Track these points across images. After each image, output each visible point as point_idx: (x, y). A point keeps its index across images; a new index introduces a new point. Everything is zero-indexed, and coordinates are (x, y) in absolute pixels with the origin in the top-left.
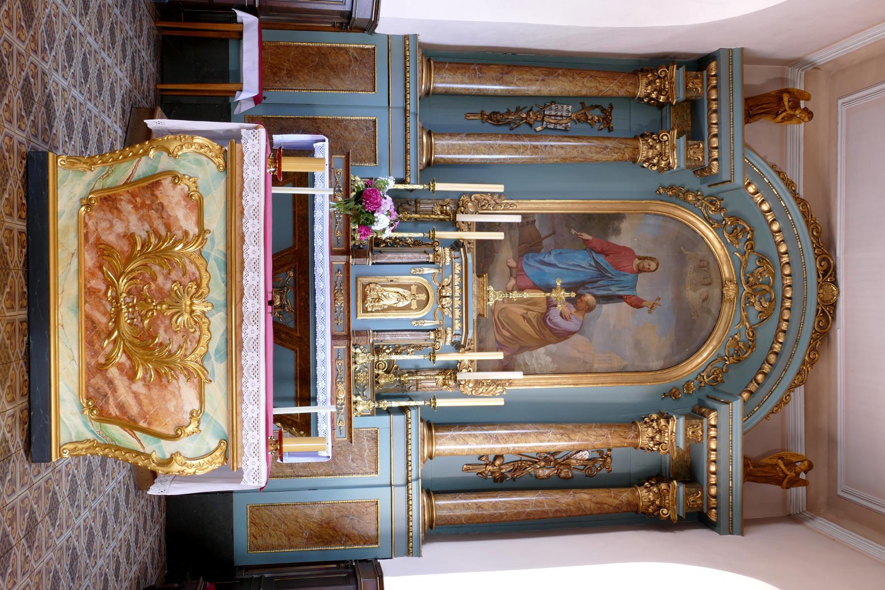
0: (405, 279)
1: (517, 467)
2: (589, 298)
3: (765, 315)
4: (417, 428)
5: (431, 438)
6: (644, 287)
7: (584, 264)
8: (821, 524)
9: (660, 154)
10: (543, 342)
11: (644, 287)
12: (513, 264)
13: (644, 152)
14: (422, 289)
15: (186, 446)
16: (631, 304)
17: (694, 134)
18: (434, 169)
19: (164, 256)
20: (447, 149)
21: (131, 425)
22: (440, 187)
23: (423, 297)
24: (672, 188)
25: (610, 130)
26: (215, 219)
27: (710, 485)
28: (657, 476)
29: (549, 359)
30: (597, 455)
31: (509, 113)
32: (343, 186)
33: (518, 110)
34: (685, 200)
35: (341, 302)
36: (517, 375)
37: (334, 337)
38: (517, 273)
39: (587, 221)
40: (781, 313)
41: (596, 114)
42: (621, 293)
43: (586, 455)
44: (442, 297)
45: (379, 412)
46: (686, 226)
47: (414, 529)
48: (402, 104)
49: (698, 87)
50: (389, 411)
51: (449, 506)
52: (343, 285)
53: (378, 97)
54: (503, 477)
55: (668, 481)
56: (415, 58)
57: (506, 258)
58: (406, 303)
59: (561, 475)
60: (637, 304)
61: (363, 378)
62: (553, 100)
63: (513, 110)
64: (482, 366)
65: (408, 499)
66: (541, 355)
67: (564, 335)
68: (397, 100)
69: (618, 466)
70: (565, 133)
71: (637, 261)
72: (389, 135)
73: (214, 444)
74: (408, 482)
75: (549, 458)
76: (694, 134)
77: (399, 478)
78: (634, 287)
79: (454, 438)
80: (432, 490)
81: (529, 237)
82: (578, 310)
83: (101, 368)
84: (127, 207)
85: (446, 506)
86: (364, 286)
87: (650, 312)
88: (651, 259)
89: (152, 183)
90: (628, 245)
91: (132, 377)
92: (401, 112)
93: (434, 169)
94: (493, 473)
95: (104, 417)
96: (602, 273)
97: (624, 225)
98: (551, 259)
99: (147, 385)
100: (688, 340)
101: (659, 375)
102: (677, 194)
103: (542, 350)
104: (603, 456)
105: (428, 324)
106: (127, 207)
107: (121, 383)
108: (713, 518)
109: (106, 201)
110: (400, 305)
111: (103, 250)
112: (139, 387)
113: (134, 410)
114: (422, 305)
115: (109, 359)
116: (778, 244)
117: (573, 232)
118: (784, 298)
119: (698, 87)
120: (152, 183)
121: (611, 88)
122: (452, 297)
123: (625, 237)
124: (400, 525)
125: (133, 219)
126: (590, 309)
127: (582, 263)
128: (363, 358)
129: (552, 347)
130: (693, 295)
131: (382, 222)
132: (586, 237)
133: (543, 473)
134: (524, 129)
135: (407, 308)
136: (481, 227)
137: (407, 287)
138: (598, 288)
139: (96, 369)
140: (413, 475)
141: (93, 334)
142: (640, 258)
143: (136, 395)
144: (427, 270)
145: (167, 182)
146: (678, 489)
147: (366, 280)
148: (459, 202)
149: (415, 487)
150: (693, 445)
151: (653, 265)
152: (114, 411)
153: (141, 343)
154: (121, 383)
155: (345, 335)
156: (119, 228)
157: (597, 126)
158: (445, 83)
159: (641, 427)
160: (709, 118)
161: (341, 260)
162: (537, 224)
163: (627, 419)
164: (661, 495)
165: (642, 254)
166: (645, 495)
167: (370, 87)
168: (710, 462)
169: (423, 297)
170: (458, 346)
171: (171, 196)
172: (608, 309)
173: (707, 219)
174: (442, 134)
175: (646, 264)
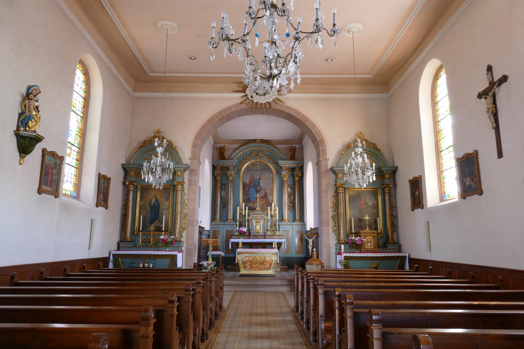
0: (255, 225)
1: (291, 203)
3: (262, 153)
4: (282, 223)
6: (257, 178)
8: (303, 143)
11: (257, 178)
13: (231, 178)
14: (256, 222)
15: (273, 259)
17: (228, 168)
18: (234, 219)
19: (251, 261)
20: (230, 216)
21: (271, 265)
22: (238, 219)
26: (248, 255)
28: (293, 176)
32: (238, 237)
35: (259, 237)
36: (273, 204)
37: (265, 238)
38: (254, 203)
41: (224, 187)
43: (289, 189)
45: (279, 230)
49: (218, 168)
50: (279, 228)
51: (297, 217)
52: (256, 237)
53: (221, 230)
55: (294, 174)
56: (214, 223)
57: (251, 205)
59: (292, 195)
60: (260, 179)
61: (273, 233)
62: (221, 195)
64: (271, 209)
66: (270, 198)
67: (266, 194)
68: (222, 226)
69: (292, 183)
70: (228, 193)
72: (229, 228)
75: (289, 197)
76: (228, 168)
77: (291, 226)
80: (294, 220)
81: (247, 200)
85: (297, 217)
89: (243, 262)
93: (234, 219)
95: (270, 268)
96: (254, 186)
97: (245, 181)
100: (268, 169)
102: (239, 171)
104: (289, 186)
109: (245, 267)
111: (251, 268)
114: (259, 222)
119: (218, 168)
120: (243, 262)
121: (219, 185)
123: (247, 181)
126: (261, 188)
127: (252, 190)
128: (269, 233)
130: (259, 168)
131: (245, 230)
133: (292, 198)
134: (226, 201)
136: (245, 209)
139: (264, 269)
141: (260, 269)
146: (296, 172)
148: (241, 214)
149: (293, 223)
153: (262, 263)
155: (265, 236)
158: (218, 217)
161: (251, 237)
163: (282, 183)
164: (296, 176)
166: (297, 179)
170: (267, 215)
171: (245, 260)
172: (261, 185)
173: (244, 165)
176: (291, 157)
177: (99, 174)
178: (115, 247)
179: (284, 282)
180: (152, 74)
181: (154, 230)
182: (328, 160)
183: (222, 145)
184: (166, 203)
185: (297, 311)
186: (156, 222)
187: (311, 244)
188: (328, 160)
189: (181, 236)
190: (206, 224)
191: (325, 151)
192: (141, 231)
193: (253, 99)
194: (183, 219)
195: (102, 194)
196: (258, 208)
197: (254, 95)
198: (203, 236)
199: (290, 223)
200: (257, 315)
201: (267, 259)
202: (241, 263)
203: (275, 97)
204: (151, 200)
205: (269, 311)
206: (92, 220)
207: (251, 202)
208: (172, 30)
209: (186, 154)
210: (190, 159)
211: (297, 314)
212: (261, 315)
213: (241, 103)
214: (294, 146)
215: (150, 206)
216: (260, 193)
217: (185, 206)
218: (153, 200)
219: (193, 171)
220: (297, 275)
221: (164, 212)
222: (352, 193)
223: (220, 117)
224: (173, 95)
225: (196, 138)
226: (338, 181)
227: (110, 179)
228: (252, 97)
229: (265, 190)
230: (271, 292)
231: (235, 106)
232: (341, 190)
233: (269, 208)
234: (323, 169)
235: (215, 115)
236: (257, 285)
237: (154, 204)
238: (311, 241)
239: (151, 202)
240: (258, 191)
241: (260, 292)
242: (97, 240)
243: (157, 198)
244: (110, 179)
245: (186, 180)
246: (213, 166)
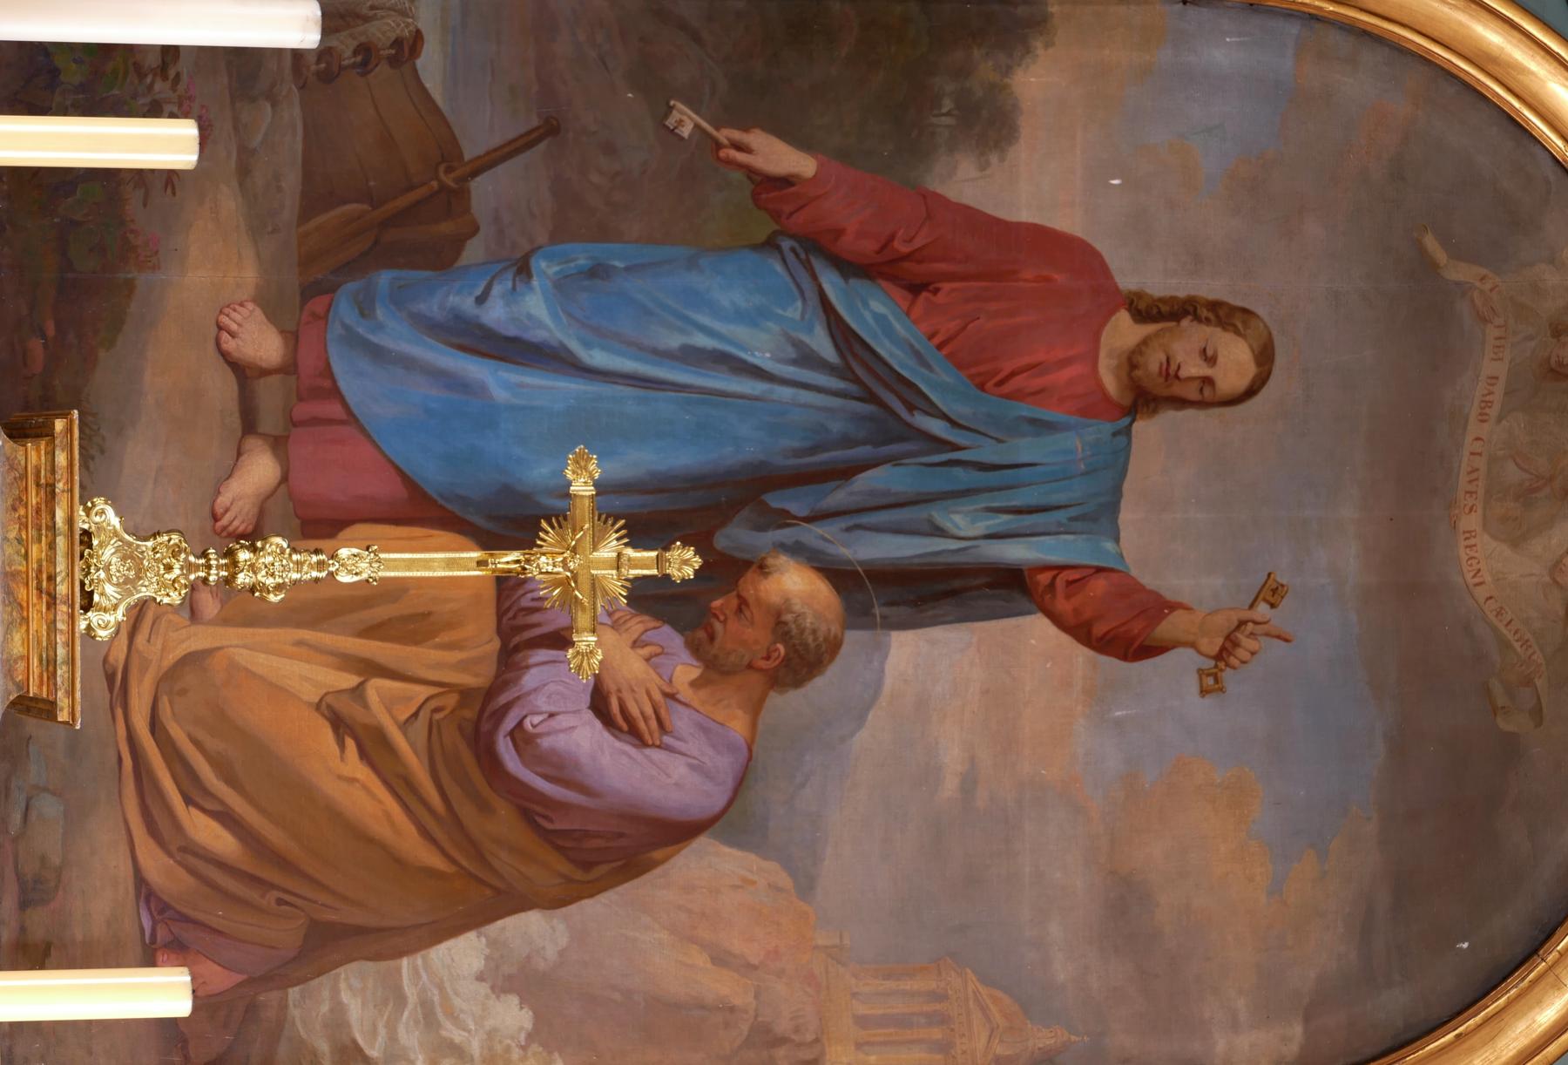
2: (794, 584)
6: (1171, 516)
11: (1171, 516)
12: (261, 342)
16: (1081, 631)
38: (288, 405)
42: (1016, 552)
57: (215, 298)
60: (1124, 628)
67: (613, 847)
71: (1123, 332)
78: (1101, 514)
82: (715, 669)
88: (1224, 315)
96: (882, 404)
98: (534, 309)
103: (463, 954)
117: (686, 120)
126: (800, 660)
129: (533, 931)
132: (776, 155)
142: (1146, 310)
151: (1234, 360)
172: (922, 660)
175: (1185, 348)
176: (48, 719)
207: (308, 289)
229: (732, 818)
236: (642, 713)
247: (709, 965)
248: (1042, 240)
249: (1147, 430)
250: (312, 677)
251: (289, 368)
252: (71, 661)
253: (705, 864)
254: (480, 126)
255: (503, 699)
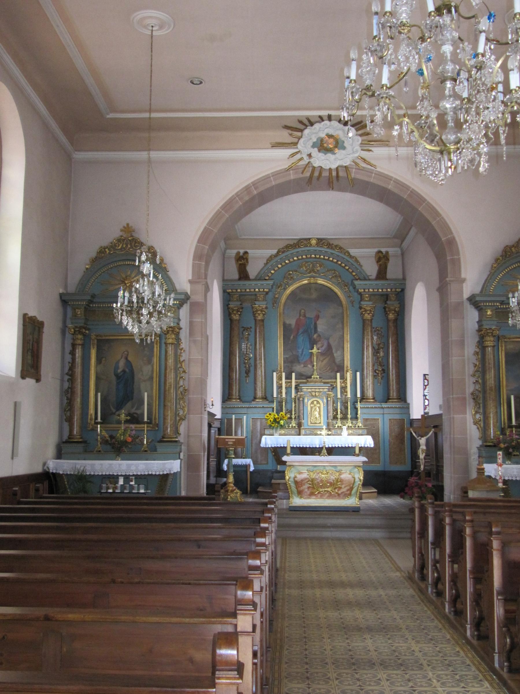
0: (309, 409)
2: (315, 336)
5: (367, 399)
7: (302, 338)
9: (262, 311)
10: (332, 354)
11: (311, 315)
12: (302, 365)
15: (357, 476)
16: (318, 320)
21: (352, 489)
23: (315, 402)
24: (273, 304)
25: (251, 328)
27: (387, 291)
29: (338, 352)
30: (376, 333)
31: (246, 367)
33: (245, 363)
34: (277, 298)
39: (286, 338)
40: (322, 259)
42: (313, 323)
44: (315, 396)
46: (288, 298)
47: (399, 406)
48: (246, 409)
51: (394, 393)
54: (383, 370)
58: (317, 408)
60: (318, 317)
63: (244, 365)
65: (389, 408)
66: (337, 355)
67: (329, 347)
71: (301, 318)
73: (357, 469)
74: (382, 408)
75: (376, 352)
77: (380, 411)
78: (311, 318)
79: (367, 390)
80: (387, 399)
82: (320, 341)
83: (339, 495)
84: (302, 488)
85: (394, 393)
86: (311, 423)
87: (320, 312)
88: (300, 311)
89: (296, 482)
90: (295, 321)
91: (340, 488)
92: (249, 409)
94: (381, 374)
96: (305, 331)
97: (288, 322)
98: (300, 350)
99: (342, 484)
101: (345, 309)
102: (275, 301)
103: (335, 355)
105: (325, 401)
106: (302, 488)
107: (342, 490)
108: (400, 290)
110: (318, 410)
112: (343, 486)
113: (348, 488)
114: (318, 402)
115: (337, 493)
116: (294, 261)
117: (290, 342)
118: (315, 258)
120: (296, 482)
122: (315, 392)
123: (292, 322)
124: (397, 411)
125: (304, 487)
126: (319, 336)
129: (334, 351)
130: (314, 295)
132: (292, 337)
135: (319, 408)
137: (312, 408)
138: (311, 333)
140: (380, 406)
142: (300, 316)
143: (345, 487)
144: (306, 401)
145: (296, 479)
147: (309, 423)
149: (384, 405)
150: (372, 296)
151: (303, 311)
152: (349, 492)
154: (342, 490)
156: (306, 490)
157: (250, 333)
159: (365, 318)
160: (248, 292)
162: (287, 356)
165: (298, 315)
167: (240, 421)
168: (378, 291)
169: (315, 402)
172: (319, 330)
173: (285, 289)
174: (255, 393)
175: (302, 314)
177: (25, 316)
178: (51, 451)
179: (376, 521)
180: (111, 116)
181: (126, 422)
182: (464, 280)
183: (242, 251)
184: (146, 369)
185: (423, 578)
186: (129, 404)
187: (423, 447)
188: (464, 280)
189: (177, 432)
190: (217, 410)
191: (457, 263)
192: (100, 423)
193: (312, 160)
194: (180, 399)
195: (29, 353)
196: (315, 376)
197: (315, 152)
198: (212, 431)
199: (378, 405)
200: (343, 585)
201: (343, 476)
202: (293, 485)
203: (357, 155)
204: (118, 362)
205: (335, 577)
206: (15, 404)
208: (161, 27)
209: (183, 275)
210: (190, 282)
211: (423, 585)
212: (351, 585)
213: (288, 170)
214: (384, 250)
215: (117, 375)
216: (319, 346)
217: (183, 375)
218: (122, 364)
219: (200, 308)
220: (423, 509)
221: (143, 386)
222: (510, 346)
223: (247, 198)
224: (155, 155)
225: (199, 241)
226: (484, 323)
227: (42, 324)
228: (310, 156)
230: (353, 539)
231: (276, 174)
232: (489, 342)
233: (338, 375)
234: (453, 299)
235: (237, 194)
237: (124, 371)
238: (423, 441)
239: (117, 367)
240: (312, 343)
241: (312, 539)
242: (25, 440)
243: (130, 359)
244: (42, 324)
245: (184, 324)
246: (224, 291)
247: (186, 420)
248: (297, 321)
249: (307, 316)
250: (320, 363)
251: (221, 420)
252: (311, 389)
253: (331, 341)
254: (291, 354)
255: (203, 442)
